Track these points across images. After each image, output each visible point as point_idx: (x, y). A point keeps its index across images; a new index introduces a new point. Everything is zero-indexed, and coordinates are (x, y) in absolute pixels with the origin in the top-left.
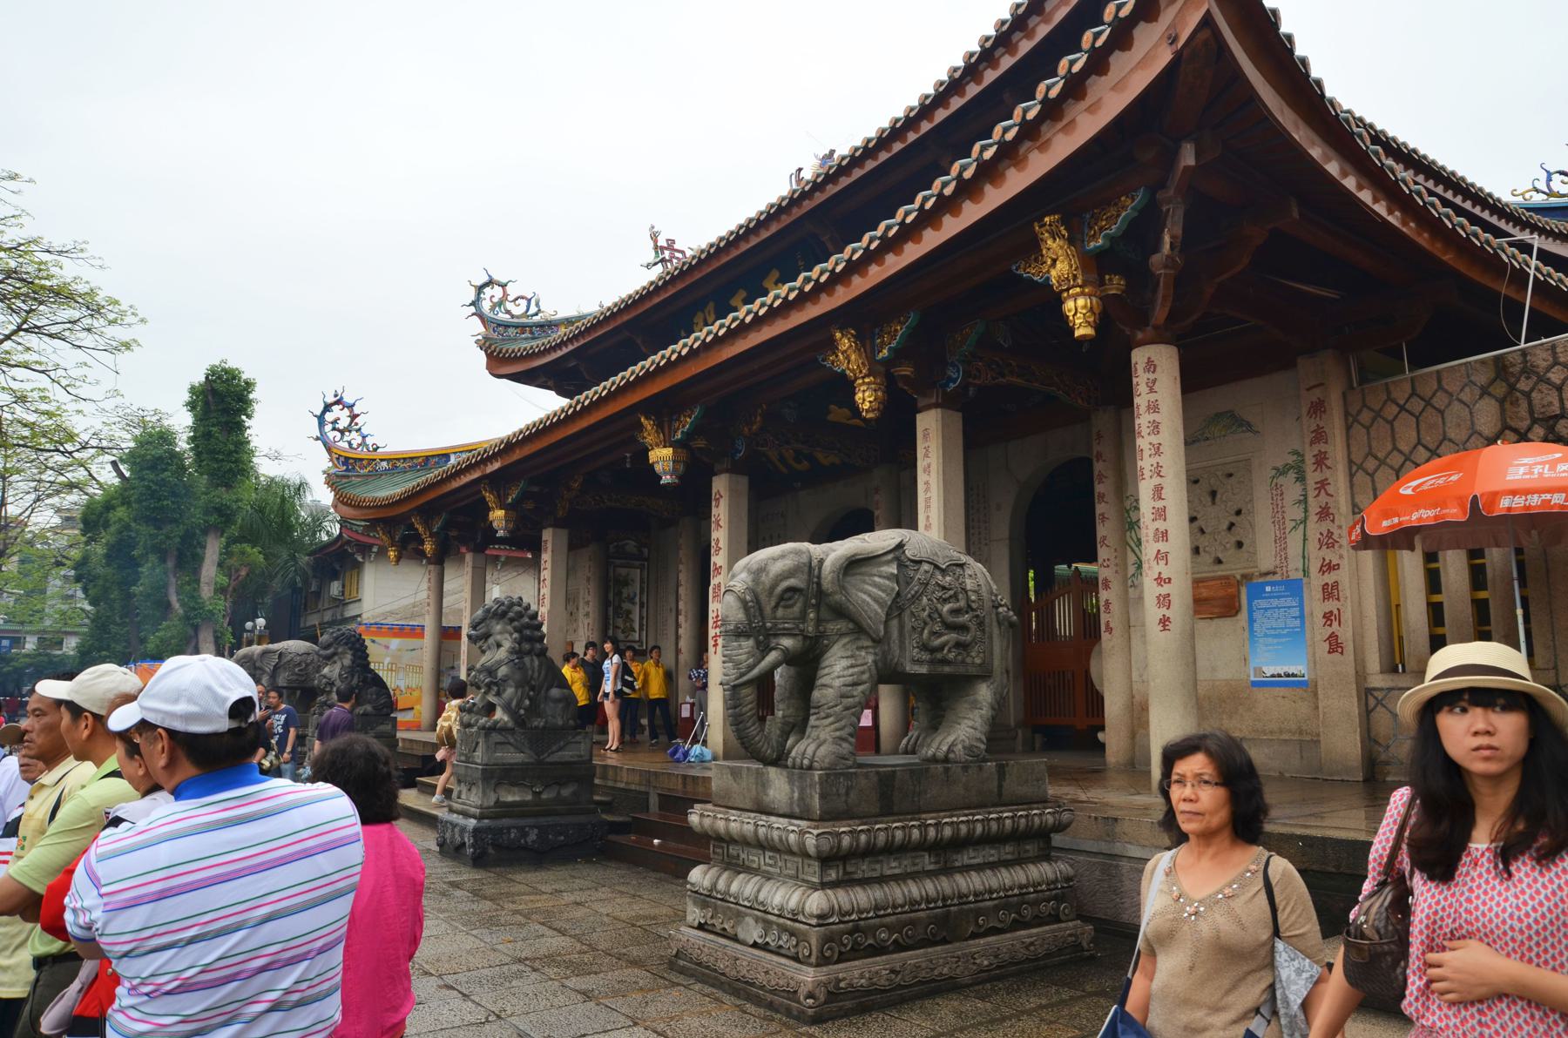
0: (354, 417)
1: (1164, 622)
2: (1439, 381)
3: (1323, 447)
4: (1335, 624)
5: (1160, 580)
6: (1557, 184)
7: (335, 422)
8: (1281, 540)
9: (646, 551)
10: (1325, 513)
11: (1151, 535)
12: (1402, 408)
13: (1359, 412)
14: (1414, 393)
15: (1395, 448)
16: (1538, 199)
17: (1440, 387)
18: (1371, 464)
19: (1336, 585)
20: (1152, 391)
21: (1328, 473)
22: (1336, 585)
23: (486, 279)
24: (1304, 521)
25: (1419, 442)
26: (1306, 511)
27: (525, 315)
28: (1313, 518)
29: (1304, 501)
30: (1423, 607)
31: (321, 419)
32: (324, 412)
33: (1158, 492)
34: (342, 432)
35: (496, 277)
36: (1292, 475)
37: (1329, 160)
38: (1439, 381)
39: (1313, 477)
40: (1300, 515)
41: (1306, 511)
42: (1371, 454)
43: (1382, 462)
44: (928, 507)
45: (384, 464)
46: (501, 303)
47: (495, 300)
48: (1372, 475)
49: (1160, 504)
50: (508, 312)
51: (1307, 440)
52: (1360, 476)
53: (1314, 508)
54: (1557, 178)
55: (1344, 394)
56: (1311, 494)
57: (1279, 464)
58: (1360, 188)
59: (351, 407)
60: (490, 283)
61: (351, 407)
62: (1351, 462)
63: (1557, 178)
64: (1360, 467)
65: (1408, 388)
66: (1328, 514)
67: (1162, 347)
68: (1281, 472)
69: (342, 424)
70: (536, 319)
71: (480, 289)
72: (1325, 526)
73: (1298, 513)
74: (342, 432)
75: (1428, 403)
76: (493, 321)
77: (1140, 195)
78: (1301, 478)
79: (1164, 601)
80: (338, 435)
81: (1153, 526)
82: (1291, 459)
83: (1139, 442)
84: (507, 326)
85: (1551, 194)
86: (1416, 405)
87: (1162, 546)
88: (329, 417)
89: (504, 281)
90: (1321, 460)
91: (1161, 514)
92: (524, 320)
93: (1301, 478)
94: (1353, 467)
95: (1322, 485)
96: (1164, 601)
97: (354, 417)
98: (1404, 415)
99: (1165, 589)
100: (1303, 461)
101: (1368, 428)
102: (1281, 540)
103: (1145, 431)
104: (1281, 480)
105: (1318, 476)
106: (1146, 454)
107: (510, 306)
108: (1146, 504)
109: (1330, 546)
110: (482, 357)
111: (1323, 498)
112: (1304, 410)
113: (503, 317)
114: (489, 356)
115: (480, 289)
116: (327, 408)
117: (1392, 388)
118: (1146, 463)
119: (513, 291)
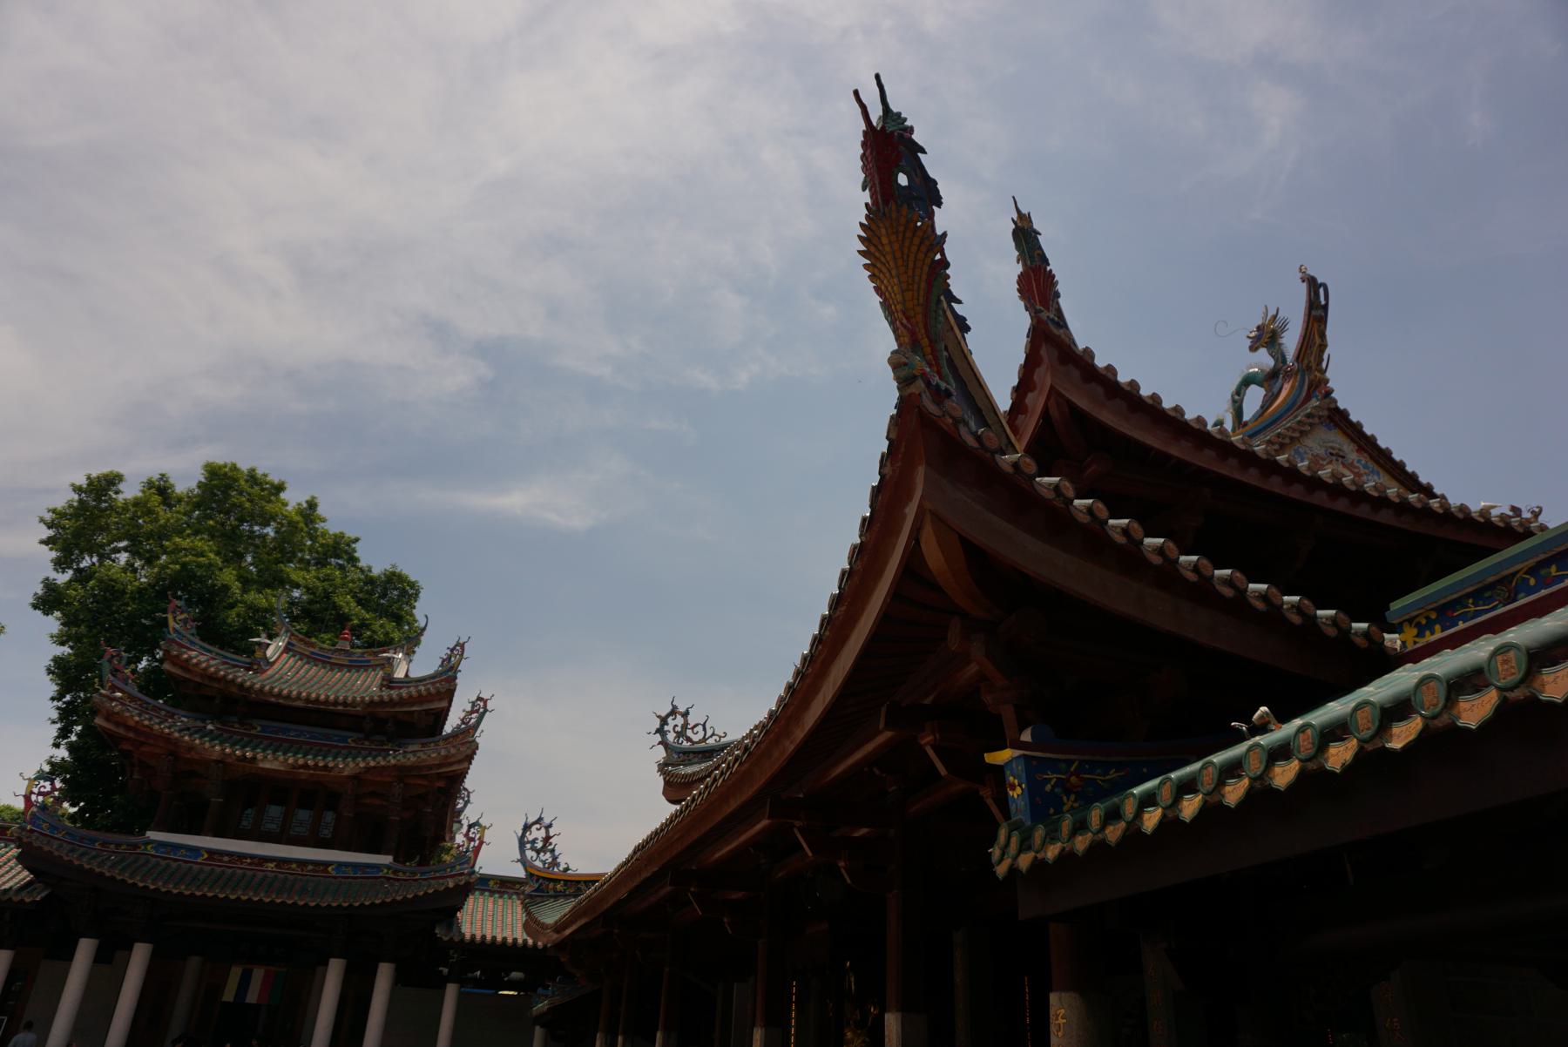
50: (689, 739)
107: (689, 733)
119: (692, 721)
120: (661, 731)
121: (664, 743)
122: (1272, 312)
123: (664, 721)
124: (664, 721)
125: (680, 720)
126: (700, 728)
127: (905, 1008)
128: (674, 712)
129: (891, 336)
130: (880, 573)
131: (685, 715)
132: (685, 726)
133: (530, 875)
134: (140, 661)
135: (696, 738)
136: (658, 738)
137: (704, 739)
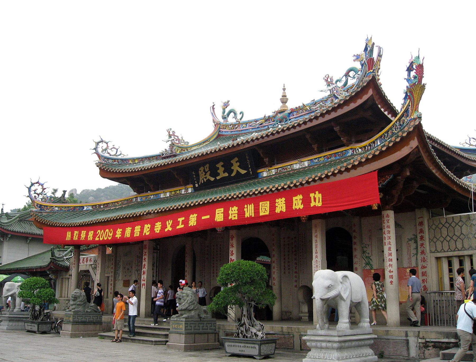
0: (44, 189)
1: (391, 282)
2: (453, 220)
3: (422, 234)
4: (425, 283)
5: (390, 271)
6: (473, 142)
7: (35, 191)
8: (410, 259)
9: (158, 246)
10: (423, 252)
11: (388, 259)
12: (443, 225)
13: (432, 225)
14: (446, 222)
15: (441, 236)
16: (467, 146)
17: (453, 221)
18: (435, 240)
19: (426, 272)
20: (388, 222)
21: (423, 242)
22: (426, 272)
23: (100, 140)
24: (417, 254)
25: (448, 235)
26: (417, 251)
27: (115, 155)
28: (419, 254)
29: (417, 248)
30: (448, 278)
31: (29, 189)
32: (31, 187)
33: (390, 249)
34: (38, 195)
35: (104, 139)
36: (413, 241)
37: (434, 169)
38: (453, 220)
39: (419, 242)
40: (415, 252)
41: (417, 251)
42: (435, 237)
43: (438, 240)
44: (316, 247)
45: (57, 208)
46: (106, 150)
47: (104, 148)
48: (435, 243)
49: (390, 252)
50: (108, 153)
51: (418, 232)
52: (432, 243)
53: (420, 251)
54: (472, 140)
55: (428, 220)
56: (419, 247)
57: (410, 238)
58: (436, 172)
59: (42, 185)
60: (102, 141)
61: (42, 185)
62: (430, 239)
63: (472, 140)
64: (432, 240)
65: (445, 220)
66: (424, 253)
67: (391, 211)
68: (410, 240)
69: (38, 192)
70: (120, 157)
71: (98, 143)
72: (423, 256)
73: (415, 252)
74: (38, 195)
75: (450, 225)
76: (103, 156)
77: (392, 176)
78: (416, 242)
79: (391, 277)
80: (37, 196)
81: (388, 258)
82: (413, 237)
83: (384, 235)
84: (108, 159)
85: (470, 145)
86: (447, 225)
87: (391, 263)
88: (33, 188)
89: (107, 141)
90: (422, 238)
91: (390, 254)
92: (115, 157)
93: (416, 242)
94: (431, 240)
95: (422, 245)
96: (391, 277)
97: (44, 189)
98: (444, 227)
99: (391, 274)
100: (417, 237)
101: (434, 230)
102: (410, 259)
103: (386, 233)
104: (410, 242)
105: (421, 242)
106: (386, 239)
107: (109, 151)
108: (386, 252)
109: (424, 261)
110: (98, 170)
111: (422, 248)
112: (417, 224)
113: (107, 155)
114: (100, 169)
115: (98, 143)
116: (32, 184)
117: (441, 219)
118: (386, 241)
119: (110, 146)
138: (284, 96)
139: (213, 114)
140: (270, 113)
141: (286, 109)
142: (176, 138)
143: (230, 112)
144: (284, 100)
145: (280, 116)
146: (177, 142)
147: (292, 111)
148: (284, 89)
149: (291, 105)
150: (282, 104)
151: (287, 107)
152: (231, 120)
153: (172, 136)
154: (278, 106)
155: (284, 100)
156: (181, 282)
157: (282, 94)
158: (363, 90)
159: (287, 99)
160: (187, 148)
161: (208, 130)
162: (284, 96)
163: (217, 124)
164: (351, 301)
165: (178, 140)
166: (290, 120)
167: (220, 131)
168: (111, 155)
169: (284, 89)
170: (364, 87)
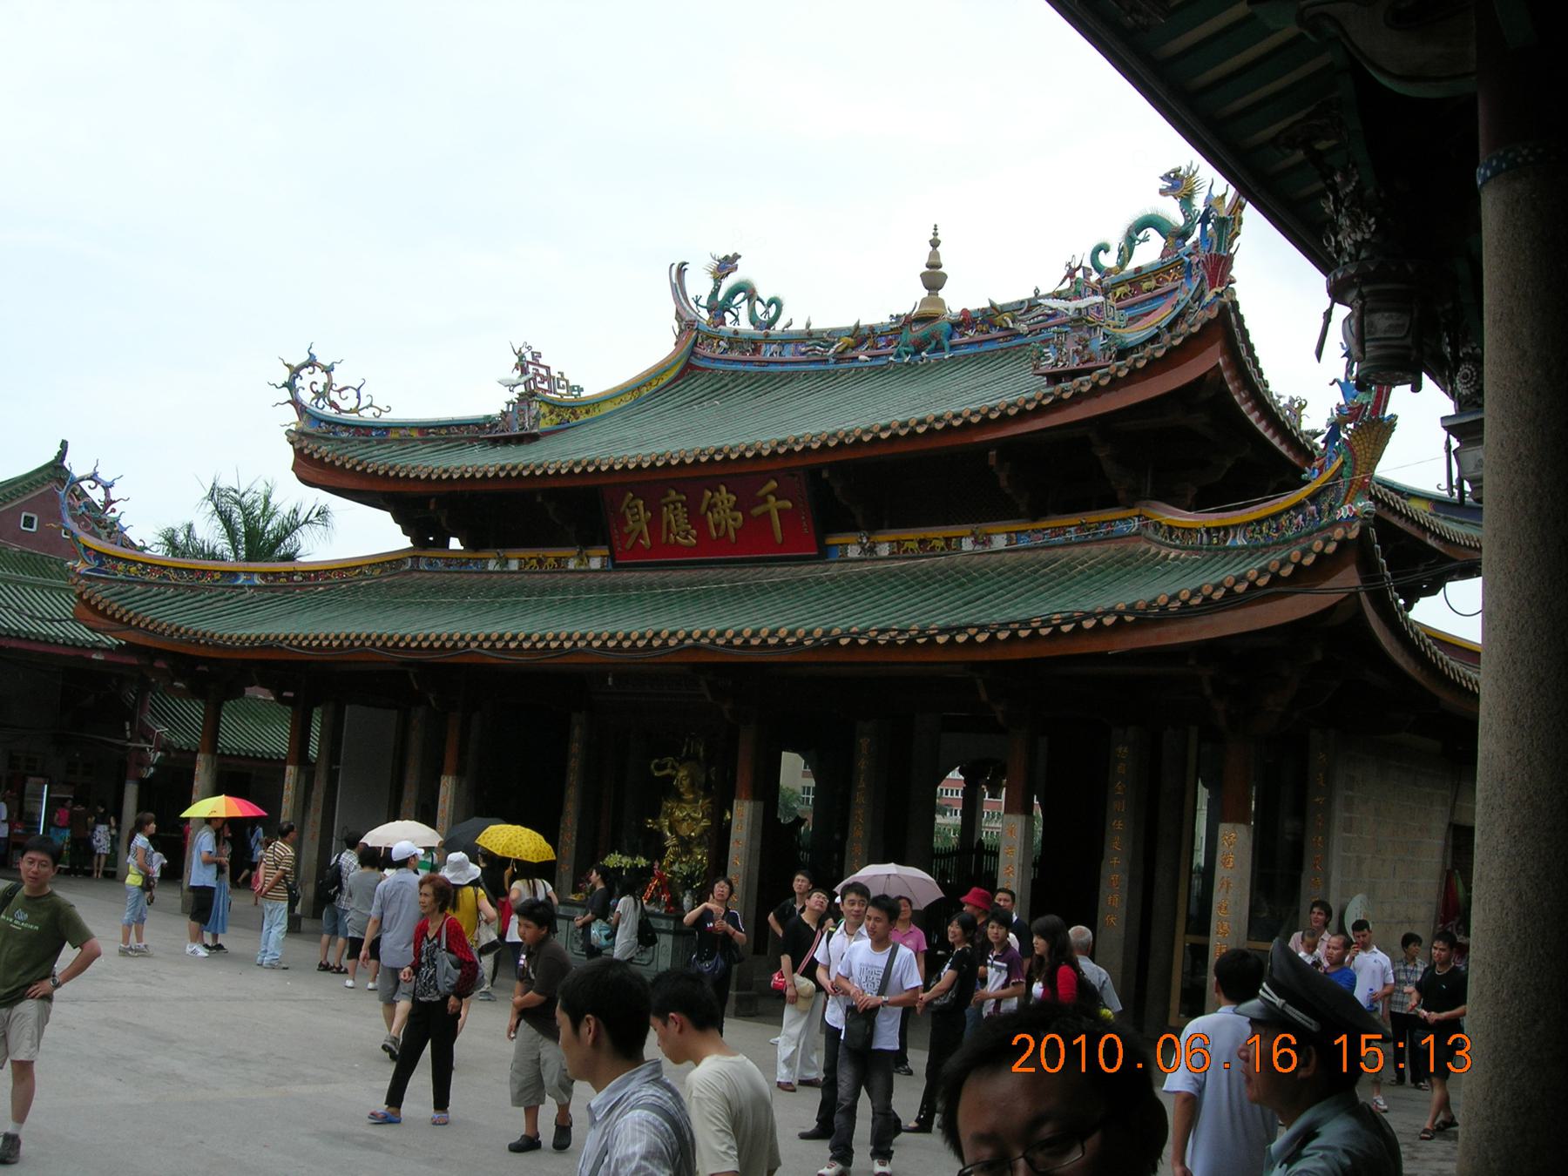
50: (333, 405)
107: (334, 396)
110: (289, 455)
113: (329, 412)
114: (299, 453)
119: (339, 379)
120: (290, 385)
121: (296, 402)
122: (699, 285)
123: (295, 372)
124: (295, 372)
125: (321, 378)
126: (352, 394)
127: (459, 773)
128: (312, 363)
129: (824, 321)
130: (1396, 645)
131: (328, 370)
132: (329, 386)
133: (70, 827)
134: (1066, 1151)
135: (344, 405)
136: (286, 394)
137: (356, 410)
138: (934, 265)
139: (679, 288)
140: (877, 314)
141: (939, 310)
142: (543, 371)
143: (733, 292)
144: (934, 279)
145: (919, 331)
146: (545, 386)
147: (967, 320)
148: (935, 243)
149: (959, 298)
150: (925, 293)
151: (941, 303)
152: (740, 321)
153: (531, 367)
154: (908, 298)
155: (934, 279)
156: (74, 569)
157: (926, 260)
158: (1192, 345)
159: (944, 277)
160: (573, 408)
161: (656, 345)
162: (934, 265)
163: (687, 325)
164: (721, 1032)
165: (548, 378)
166: (953, 347)
167: (693, 353)
168: (341, 411)
169: (935, 243)
170: (1192, 335)
